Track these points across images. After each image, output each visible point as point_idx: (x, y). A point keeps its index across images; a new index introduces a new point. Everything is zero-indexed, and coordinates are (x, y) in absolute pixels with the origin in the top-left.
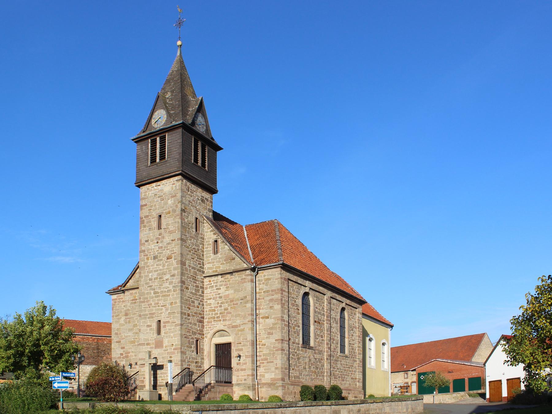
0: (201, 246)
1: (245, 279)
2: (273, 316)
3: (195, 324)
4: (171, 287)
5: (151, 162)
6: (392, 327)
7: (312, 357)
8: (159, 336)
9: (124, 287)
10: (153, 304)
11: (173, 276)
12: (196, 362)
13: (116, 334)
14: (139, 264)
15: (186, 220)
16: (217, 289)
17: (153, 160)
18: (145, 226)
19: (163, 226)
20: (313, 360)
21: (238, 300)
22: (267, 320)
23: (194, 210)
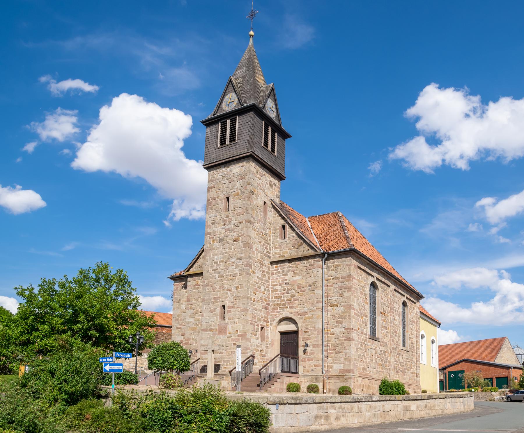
1: (314, 265)
3: (261, 310)
4: (237, 271)
5: (221, 145)
6: (439, 324)
7: (378, 349)
8: (223, 322)
9: (188, 271)
10: (217, 288)
11: (240, 259)
12: (261, 350)
13: (177, 320)
14: (205, 247)
15: (255, 203)
16: (284, 275)
17: (223, 142)
18: (212, 209)
19: (231, 208)
20: (379, 352)
21: (306, 287)
22: (336, 308)
23: (263, 194)
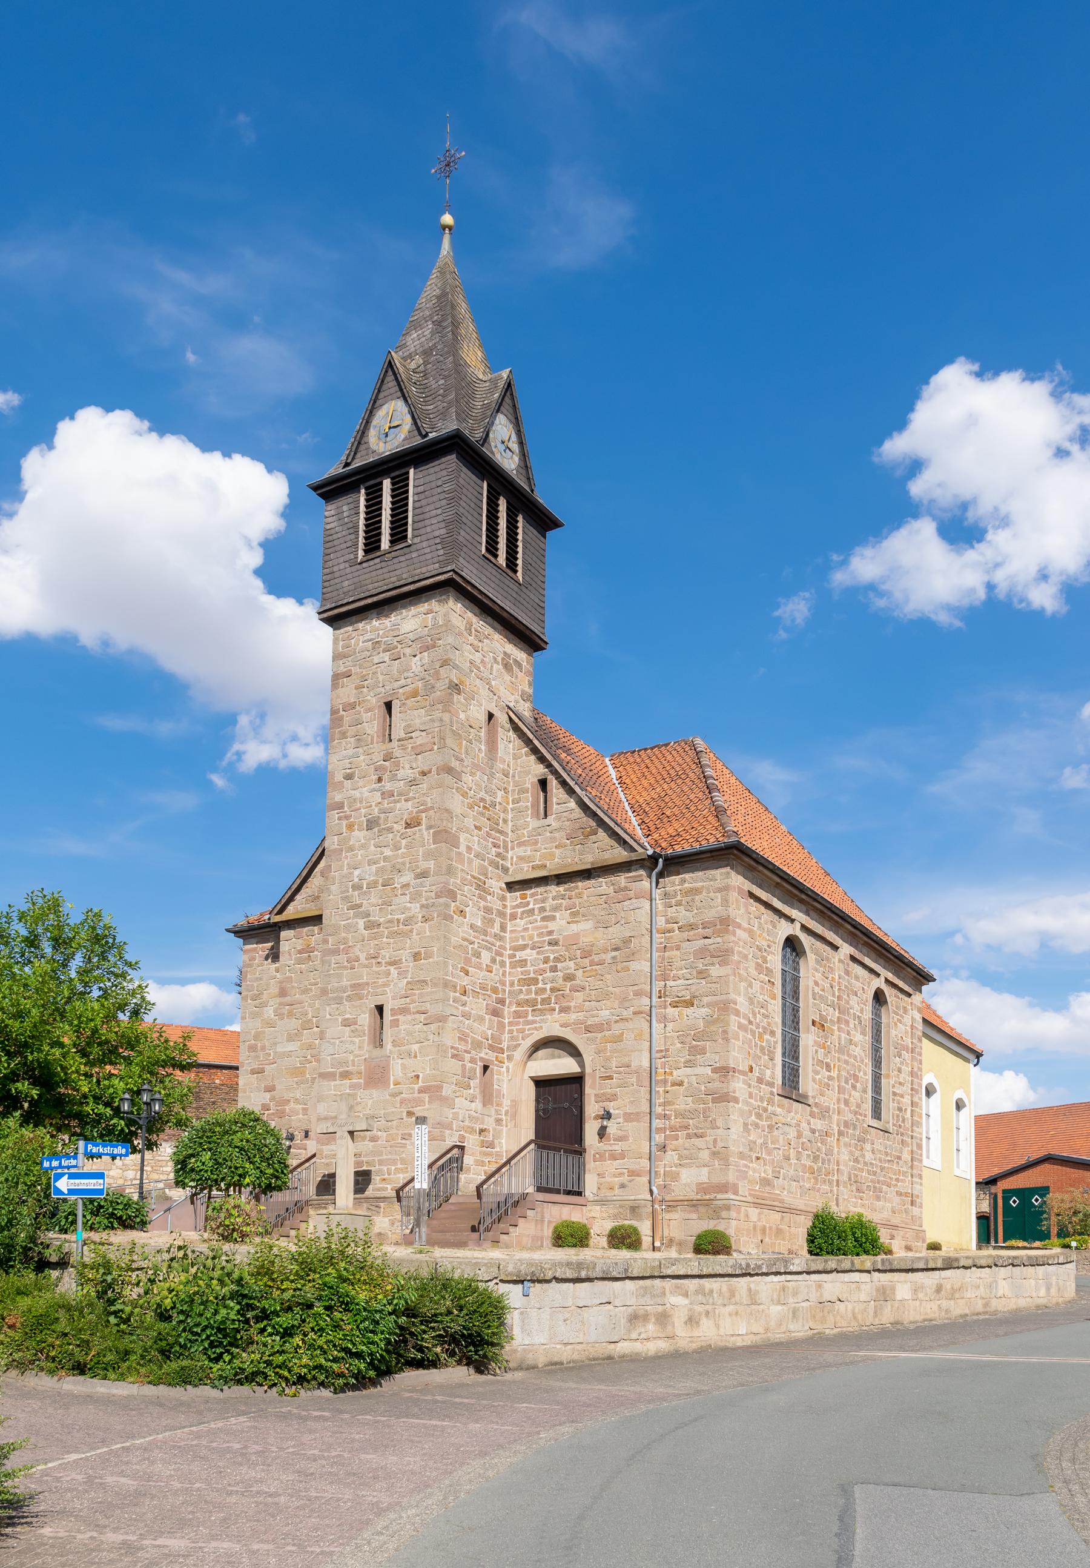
0: (500, 794)
1: (626, 889)
2: (706, 1000)
3: (481, 1019)
4: (415, 908)
5: (366, 552)
6: (978, 1055)
7: (804, 1125)
9: (280, 912)
10: (362, 957)
11: (424, 875)
12: (482, 1131)
14: (326, 844)
16: (544, 919)
18: (344, 735)
19: (398, 732)
20: (807, 1133)
22: (690, 1011)
23: (484, 692)
